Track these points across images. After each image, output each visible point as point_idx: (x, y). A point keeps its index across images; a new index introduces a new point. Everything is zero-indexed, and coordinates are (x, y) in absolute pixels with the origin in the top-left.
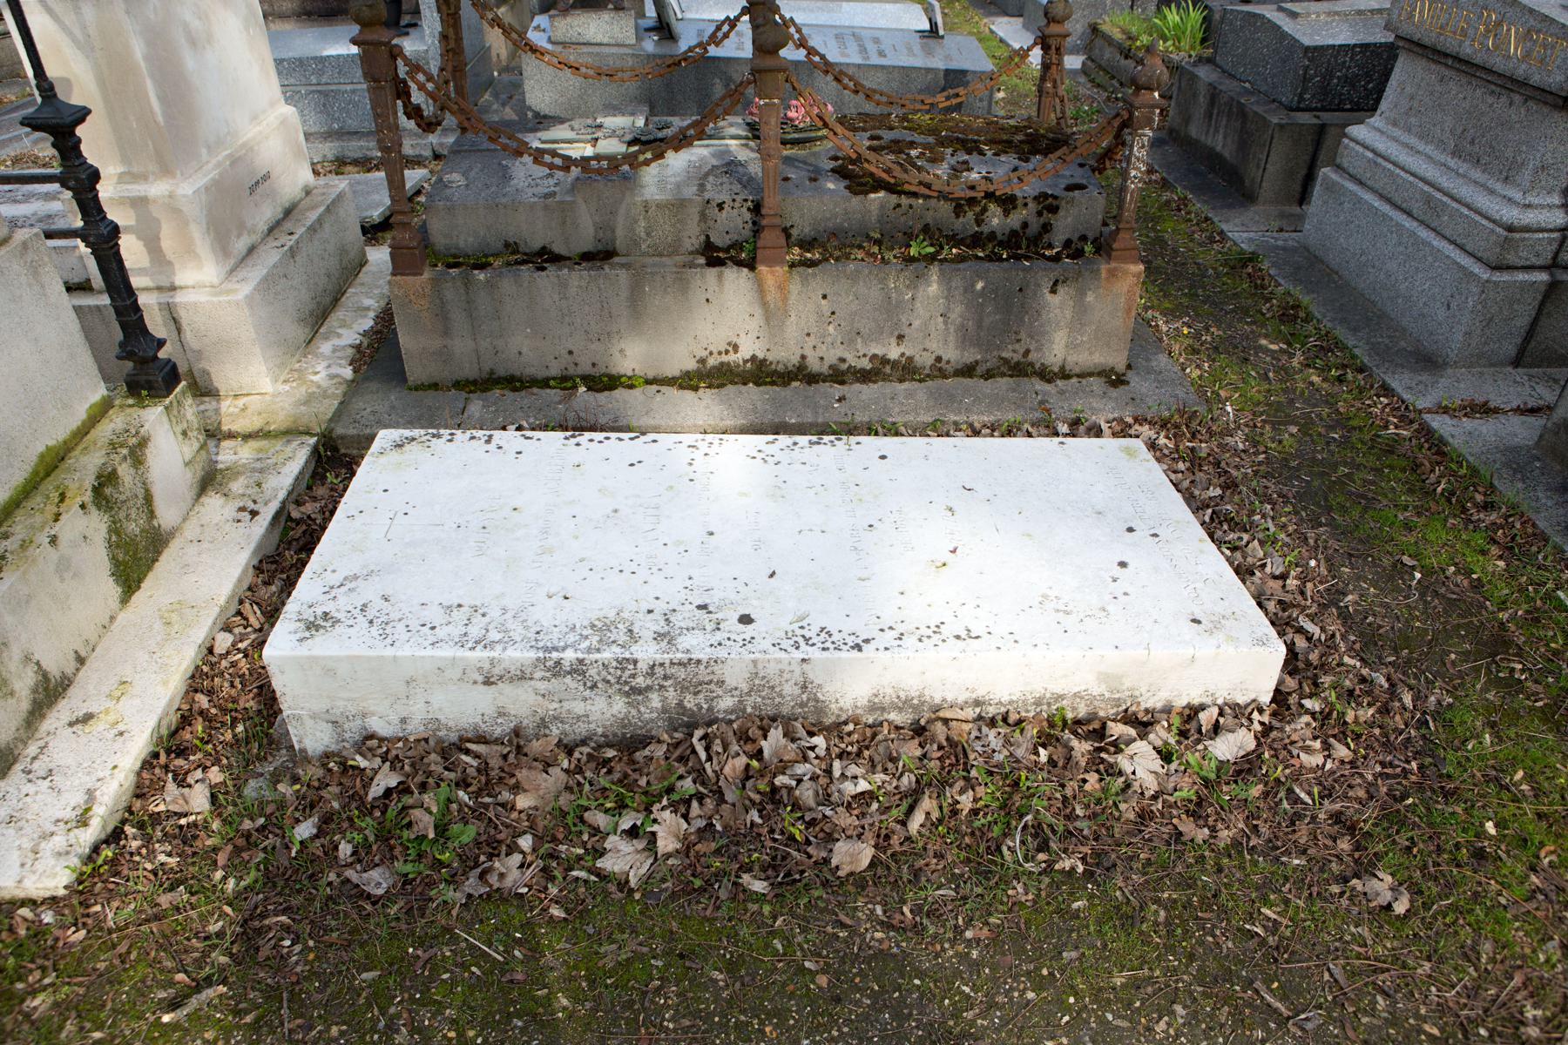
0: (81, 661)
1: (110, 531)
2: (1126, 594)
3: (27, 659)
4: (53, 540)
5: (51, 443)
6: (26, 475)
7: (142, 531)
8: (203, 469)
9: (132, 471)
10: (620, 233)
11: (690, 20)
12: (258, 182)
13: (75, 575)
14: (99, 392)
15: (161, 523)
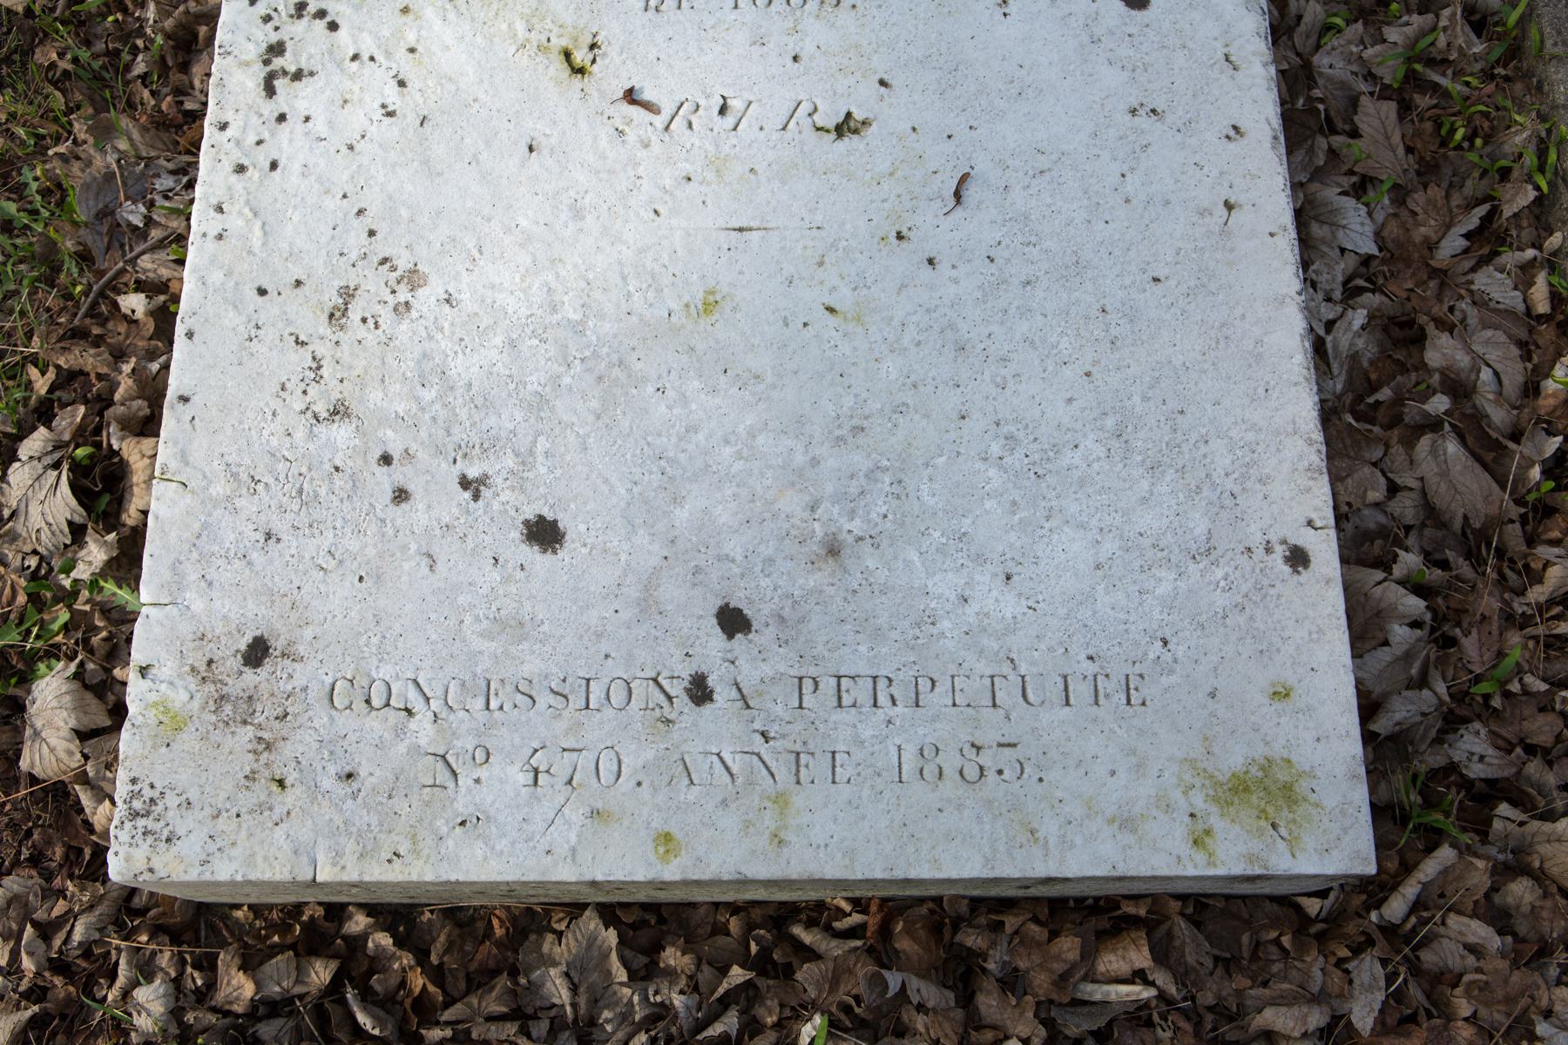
2: (401, 495)
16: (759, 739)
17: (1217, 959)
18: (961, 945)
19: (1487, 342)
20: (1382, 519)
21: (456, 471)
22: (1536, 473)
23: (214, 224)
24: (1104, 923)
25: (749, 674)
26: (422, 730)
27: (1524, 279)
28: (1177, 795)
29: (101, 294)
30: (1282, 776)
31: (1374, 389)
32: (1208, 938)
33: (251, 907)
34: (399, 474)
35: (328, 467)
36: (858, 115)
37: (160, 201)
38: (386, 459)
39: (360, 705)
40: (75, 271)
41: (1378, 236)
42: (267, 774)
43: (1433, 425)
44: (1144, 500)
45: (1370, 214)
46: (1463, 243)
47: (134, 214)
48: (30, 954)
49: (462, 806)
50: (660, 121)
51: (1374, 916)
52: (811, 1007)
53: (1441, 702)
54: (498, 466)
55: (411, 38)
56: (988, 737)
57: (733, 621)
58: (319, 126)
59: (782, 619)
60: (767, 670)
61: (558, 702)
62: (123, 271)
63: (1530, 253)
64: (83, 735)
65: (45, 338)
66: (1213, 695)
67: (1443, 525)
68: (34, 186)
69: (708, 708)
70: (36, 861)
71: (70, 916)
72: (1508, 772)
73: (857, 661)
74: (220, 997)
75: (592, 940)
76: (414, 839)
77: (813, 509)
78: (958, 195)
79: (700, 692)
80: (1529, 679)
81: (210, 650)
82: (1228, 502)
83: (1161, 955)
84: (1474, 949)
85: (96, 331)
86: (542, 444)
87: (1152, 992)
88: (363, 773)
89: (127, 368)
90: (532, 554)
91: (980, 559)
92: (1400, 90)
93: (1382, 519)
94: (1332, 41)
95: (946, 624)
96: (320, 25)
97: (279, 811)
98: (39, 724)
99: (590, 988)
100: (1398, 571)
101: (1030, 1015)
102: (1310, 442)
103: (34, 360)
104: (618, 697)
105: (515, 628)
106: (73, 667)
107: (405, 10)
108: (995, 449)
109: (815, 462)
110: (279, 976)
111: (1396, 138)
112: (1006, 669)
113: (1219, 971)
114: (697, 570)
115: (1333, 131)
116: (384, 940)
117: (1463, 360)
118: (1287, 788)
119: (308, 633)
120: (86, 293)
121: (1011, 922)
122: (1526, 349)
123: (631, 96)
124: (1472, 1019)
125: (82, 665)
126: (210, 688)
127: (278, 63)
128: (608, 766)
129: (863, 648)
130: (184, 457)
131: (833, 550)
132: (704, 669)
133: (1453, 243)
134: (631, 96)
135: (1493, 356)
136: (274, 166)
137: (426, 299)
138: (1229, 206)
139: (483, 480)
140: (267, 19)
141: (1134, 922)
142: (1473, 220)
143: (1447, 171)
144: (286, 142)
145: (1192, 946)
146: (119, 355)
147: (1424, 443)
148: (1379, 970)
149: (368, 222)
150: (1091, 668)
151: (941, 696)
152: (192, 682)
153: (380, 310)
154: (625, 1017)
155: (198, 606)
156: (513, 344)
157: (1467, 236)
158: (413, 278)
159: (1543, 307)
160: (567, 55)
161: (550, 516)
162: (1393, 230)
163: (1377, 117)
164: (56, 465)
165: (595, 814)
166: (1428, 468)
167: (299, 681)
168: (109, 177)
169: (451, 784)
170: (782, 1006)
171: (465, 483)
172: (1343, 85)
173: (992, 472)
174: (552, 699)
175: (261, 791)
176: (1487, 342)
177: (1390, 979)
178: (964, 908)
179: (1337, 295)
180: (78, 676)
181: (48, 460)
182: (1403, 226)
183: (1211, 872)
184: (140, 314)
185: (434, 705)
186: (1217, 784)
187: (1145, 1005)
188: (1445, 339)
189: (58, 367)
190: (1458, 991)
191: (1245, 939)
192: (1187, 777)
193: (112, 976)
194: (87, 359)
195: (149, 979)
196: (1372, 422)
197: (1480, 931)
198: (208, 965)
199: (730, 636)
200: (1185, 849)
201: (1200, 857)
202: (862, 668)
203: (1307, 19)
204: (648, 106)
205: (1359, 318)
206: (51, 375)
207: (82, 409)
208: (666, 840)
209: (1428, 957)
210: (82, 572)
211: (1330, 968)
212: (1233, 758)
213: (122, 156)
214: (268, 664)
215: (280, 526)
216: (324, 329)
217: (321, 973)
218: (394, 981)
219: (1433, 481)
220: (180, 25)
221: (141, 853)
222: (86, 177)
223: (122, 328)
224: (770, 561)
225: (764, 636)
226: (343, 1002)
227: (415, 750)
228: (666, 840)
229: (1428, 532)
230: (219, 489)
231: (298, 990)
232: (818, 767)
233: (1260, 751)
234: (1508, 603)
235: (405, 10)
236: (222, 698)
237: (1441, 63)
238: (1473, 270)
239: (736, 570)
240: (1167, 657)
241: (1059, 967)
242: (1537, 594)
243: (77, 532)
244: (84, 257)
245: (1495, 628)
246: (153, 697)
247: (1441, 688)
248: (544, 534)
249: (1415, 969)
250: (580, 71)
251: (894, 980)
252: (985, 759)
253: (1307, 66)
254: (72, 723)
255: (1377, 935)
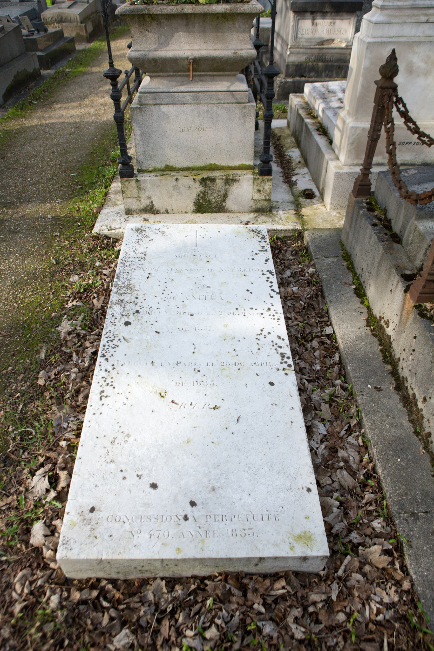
0: (167, 212)
1: (201, 192)
2: (124, 478)
3: (149, 198)
4: (177, 180)
5: (217, 163)
6: (202, 166)
7: (215, 202)
8: (262, 206)
9: (223, 184)
10: (406, 234)
11: (96, 73)
12: (411, 143)
13: (179, 192)
14: (251, 163)
15: (227, 206)
16: (198, 528)
17: (301, 585)
18: (243, 583)
19: (351, 451)
20: (331, 488)
21: (136, 473)
22: (362, 477)
23: (88, 424)
24: (276, 578)
25: (196, 515)
26: (127, 526)
27: (357, 439)
28: (286, 539)
29: (56, 442)
30: (308, 535)
31: (328, 461)
32: (299, 580)
33: (78, 580)
34: (124, 474)
35: (109, 472)
36: (218, 406)
37: (70, 422)
38: (122, 471)
39: (114, 521)
40: (51, 436)
41: (327, 431)
42: (93, 535)
43: (341, 468)
44: (277, 479)
45: (325, 426)
46: (345, 432)
47: (65, 425)
48: (27, 588)
49: (135, 542)
50: (178, 406)
51: (336, 574)
52: (209, 596)
53: (346, 526)
54: (144, 473)
55: (129, 390)
56: (246, 527)
57: (193, 504)
58: (110, 406)
59: (203, 503)
60: (200, 514)
61: (156, 520)
62: (61, 437)
63: (358, 433)
64: (46, 536)
65: (44, 450)
66: (293, 518)
67: (344, 489)
68: (42, 420)
69: (187, 522)
70: (30, 566)
71: (37, 579)
72: (362, 541)
73: (219, 512)
74: (71, 598)
75: (159, 585)
76: (124, 549)
77: (209, 481)
78: (238, 421)
79: (186, 518)
80: (364, 520)
81: (83, 509)
82: (294, 479)
83: (289, 583)
84: (358, 581)
85: (54, 449)
86: (154, 468)
87: (286, 591)
88: (114, 535)
89: (61, 457)
90: (151, 490)
91: (244, 491)
92: (330, 402)
93: (331, 488)
94: (315, 392)
95: (237, 504)
96: (112, 387)
97: (95, 544)
98: (35, 534)
99: (158, 596)
100: (334, 497)
101: (259, 597)
102: (310, 467)
103: (40, 455)
104: (169, 519)
105: (147, 505)
106: (44, 521)
107: (128, 385)
108: (246, 469)
109: (210, 472)
110: (85, 595)
111: (329, 411)
112: (250, 513)
113: (302, 588)
114: (186, 494)
115: (316, 410)
116: (110, 586)
117: (346, 455)
118: (310, 537)
119: (104, 506)
120: (53, 441)
121: (254, 577)
122: (359, 453)
123: (173, 402)
124: (359, 596)
125: (45, 521)
126: (82, 517)
127: (103, 394)
128: (166, 534)
129: (220, 509)
130: (79, 470)
131: (213, 489)
132: (187, 514)
133: (343, 432)
134: (173, 402)
135: (352, 454)
136: (101, 413)
137: (131, 440)
138: (292, 422)
139: (141, 475)
140: (101, 386)
141: (281, 577)
142: (346, 428)
143: (340, 418)
144: (103, 409)
145: (295, 582)
146: (59, 454)
147: (338, 471)
148: (337, 586)
149: (119, 425)
150: (267, 513)
151: (236, 519)
152: (78, 516)
153: (121, 441)
154: (166, 601)
155: (80, 500)
156: (148, 449)
157: (346, 430)
158: (128, 436)
159: (361, 444)
160: (160, 394)
161: (155, 483)
162: (330, 430)
163: (325, 407)
164: (44, 476)
165: (163, 544)
166: (339, 476)
167: (101, 516)
168: (61, 417)
169: (132, 537)
170: (203, 597)
171: (138, 476)
172: (318, 401)
173: (246, 474)
174: (155, 520)
175: (92, 538)
176: (351, 451)
177: (339, 587)
178: (244, 575)
179: (319, 442)
180: (45, 523)
181: (43, 475)
182: (332, 429)
183: (294, 555)
184: (64, 446)
185: (130, 521)
186: (295, 537)
187: (284, 594)
188: (342, 451)
189: (46, 456)
190: (355, 590)
191: (307, 580)
192: (288, 535)
193: (45, 594)
194: (52, 454)
195: (55, 594)
196: (328, 468)
197: (359, 577)
198: (69, 591)
199: (192, 507)
200: (289, 550)
201: (292, 552)
202: (220, 513)
203: (309, 388)
204: (176, 404)
205: (323, 446)
206: (44, 458)
207: (51, 465)
208: (178, 550)
209: (348, 583)
210: (48, 499)
211: (327, 587)
212: (298, 531)
213: (64, 413)
214: (95, 512)
215: (98, 484)
216: (109, 444)
217: (95, 593)
218: (112, 596)
219: (341, 479)
220: (78, 388)
221: (64, 552)
222: (56, 417)
223: (60, 449)
224: (201, 492)
225: (199, 507)
226: (99, 601)
227: (125, 530)
228: (178, 550)
229: (341, 490)
230: (86, 476)
231: (89, 597)
232: (211, 534)
233: (303, 530)
234: (358, 504)
235: (128, 385)
236: (84, 519)
237: (336, 397)
238: (347, 437)
239: (193, 493)
240: (283, 510)
241: (265, 587)
242: (364, 501)
243: (48, 491)
244: (53, 434)
245: (355, 509)
246: (69, 519)
247: (346, 523)
248: (154, 486)
249: (346, 586)
250: (163, 397)
251: (228, 586)
252: (246, 532)
253: (310, 397)
254: (43, 533)
255: (336, 578)
